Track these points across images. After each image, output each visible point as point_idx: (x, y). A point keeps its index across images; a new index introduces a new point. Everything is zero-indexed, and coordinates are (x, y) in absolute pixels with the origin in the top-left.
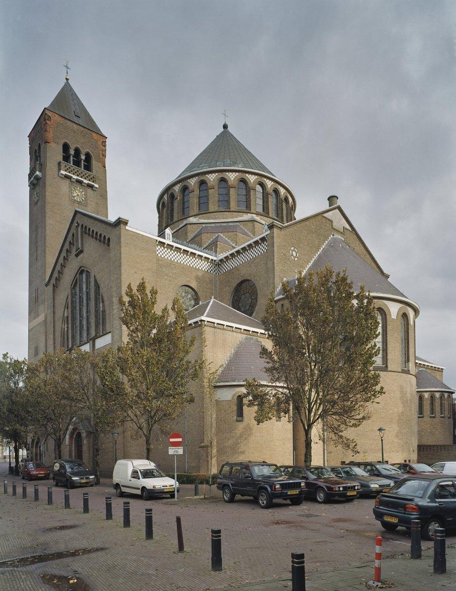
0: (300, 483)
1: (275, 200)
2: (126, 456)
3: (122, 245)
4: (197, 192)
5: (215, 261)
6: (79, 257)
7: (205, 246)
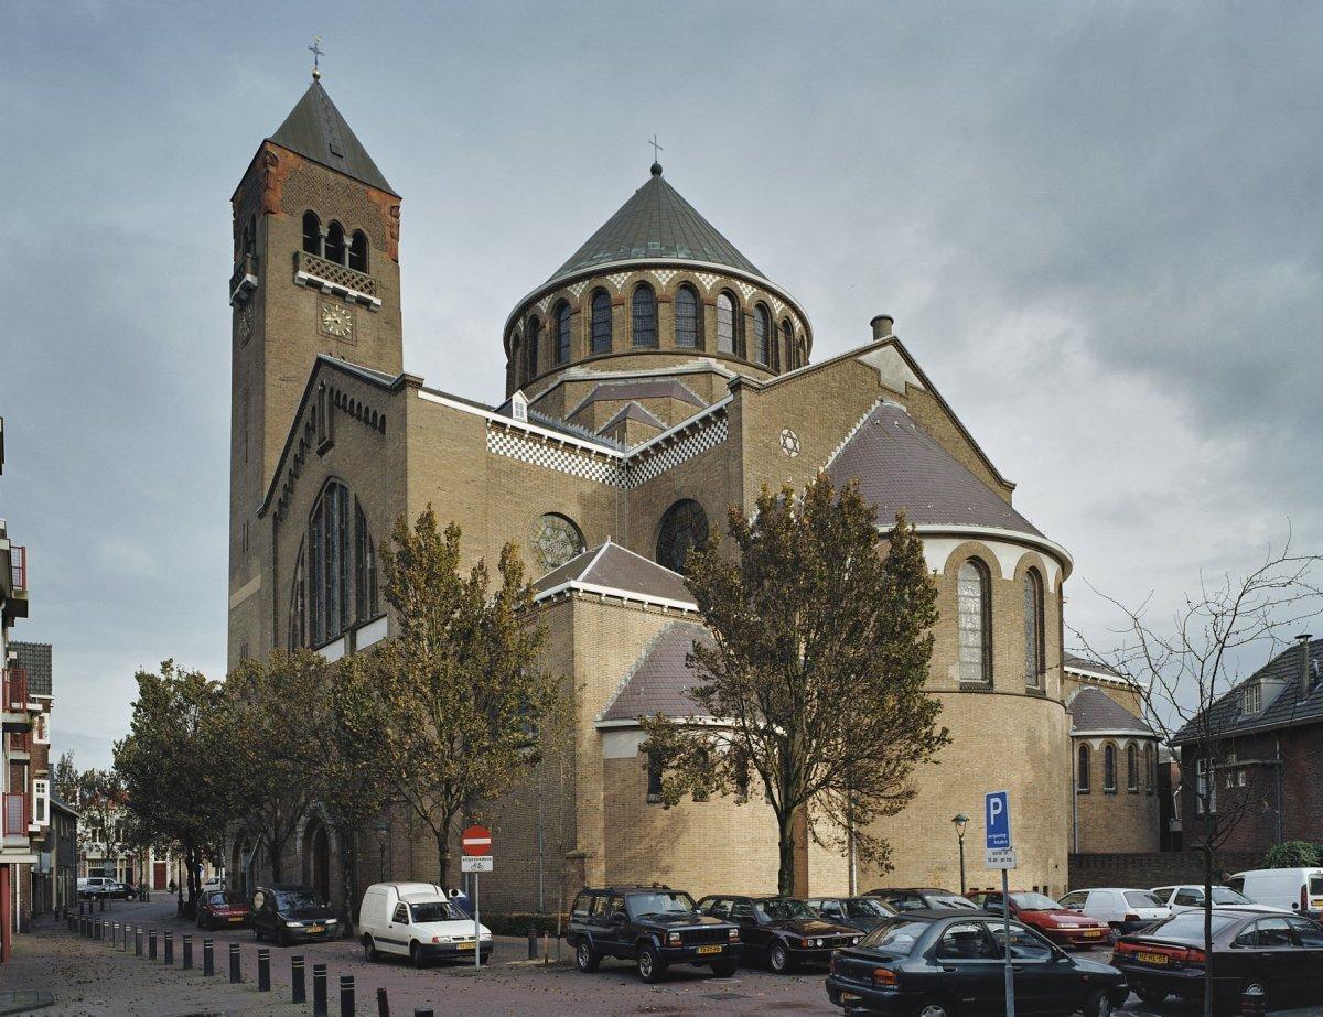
0: (727, 931)
1: (760, 328)
2: (387, 877)
3: (410, 430)
4: (587, 312)
5: (620, 460)
6: (324, 457)
7: (601, 428)
